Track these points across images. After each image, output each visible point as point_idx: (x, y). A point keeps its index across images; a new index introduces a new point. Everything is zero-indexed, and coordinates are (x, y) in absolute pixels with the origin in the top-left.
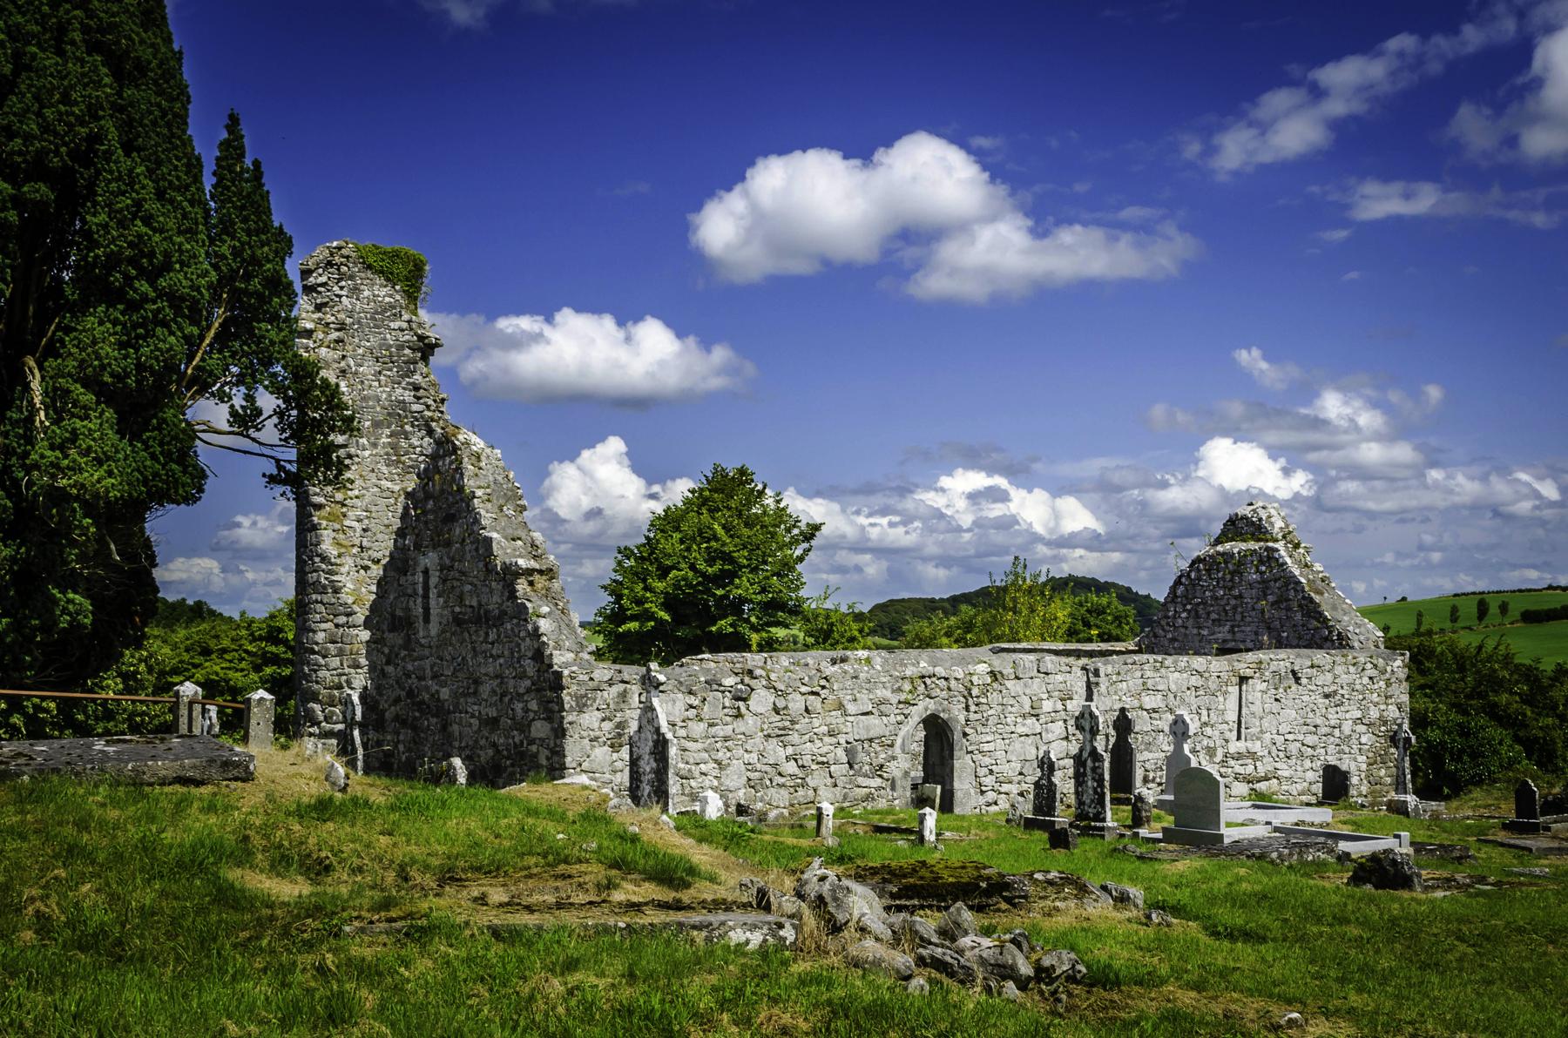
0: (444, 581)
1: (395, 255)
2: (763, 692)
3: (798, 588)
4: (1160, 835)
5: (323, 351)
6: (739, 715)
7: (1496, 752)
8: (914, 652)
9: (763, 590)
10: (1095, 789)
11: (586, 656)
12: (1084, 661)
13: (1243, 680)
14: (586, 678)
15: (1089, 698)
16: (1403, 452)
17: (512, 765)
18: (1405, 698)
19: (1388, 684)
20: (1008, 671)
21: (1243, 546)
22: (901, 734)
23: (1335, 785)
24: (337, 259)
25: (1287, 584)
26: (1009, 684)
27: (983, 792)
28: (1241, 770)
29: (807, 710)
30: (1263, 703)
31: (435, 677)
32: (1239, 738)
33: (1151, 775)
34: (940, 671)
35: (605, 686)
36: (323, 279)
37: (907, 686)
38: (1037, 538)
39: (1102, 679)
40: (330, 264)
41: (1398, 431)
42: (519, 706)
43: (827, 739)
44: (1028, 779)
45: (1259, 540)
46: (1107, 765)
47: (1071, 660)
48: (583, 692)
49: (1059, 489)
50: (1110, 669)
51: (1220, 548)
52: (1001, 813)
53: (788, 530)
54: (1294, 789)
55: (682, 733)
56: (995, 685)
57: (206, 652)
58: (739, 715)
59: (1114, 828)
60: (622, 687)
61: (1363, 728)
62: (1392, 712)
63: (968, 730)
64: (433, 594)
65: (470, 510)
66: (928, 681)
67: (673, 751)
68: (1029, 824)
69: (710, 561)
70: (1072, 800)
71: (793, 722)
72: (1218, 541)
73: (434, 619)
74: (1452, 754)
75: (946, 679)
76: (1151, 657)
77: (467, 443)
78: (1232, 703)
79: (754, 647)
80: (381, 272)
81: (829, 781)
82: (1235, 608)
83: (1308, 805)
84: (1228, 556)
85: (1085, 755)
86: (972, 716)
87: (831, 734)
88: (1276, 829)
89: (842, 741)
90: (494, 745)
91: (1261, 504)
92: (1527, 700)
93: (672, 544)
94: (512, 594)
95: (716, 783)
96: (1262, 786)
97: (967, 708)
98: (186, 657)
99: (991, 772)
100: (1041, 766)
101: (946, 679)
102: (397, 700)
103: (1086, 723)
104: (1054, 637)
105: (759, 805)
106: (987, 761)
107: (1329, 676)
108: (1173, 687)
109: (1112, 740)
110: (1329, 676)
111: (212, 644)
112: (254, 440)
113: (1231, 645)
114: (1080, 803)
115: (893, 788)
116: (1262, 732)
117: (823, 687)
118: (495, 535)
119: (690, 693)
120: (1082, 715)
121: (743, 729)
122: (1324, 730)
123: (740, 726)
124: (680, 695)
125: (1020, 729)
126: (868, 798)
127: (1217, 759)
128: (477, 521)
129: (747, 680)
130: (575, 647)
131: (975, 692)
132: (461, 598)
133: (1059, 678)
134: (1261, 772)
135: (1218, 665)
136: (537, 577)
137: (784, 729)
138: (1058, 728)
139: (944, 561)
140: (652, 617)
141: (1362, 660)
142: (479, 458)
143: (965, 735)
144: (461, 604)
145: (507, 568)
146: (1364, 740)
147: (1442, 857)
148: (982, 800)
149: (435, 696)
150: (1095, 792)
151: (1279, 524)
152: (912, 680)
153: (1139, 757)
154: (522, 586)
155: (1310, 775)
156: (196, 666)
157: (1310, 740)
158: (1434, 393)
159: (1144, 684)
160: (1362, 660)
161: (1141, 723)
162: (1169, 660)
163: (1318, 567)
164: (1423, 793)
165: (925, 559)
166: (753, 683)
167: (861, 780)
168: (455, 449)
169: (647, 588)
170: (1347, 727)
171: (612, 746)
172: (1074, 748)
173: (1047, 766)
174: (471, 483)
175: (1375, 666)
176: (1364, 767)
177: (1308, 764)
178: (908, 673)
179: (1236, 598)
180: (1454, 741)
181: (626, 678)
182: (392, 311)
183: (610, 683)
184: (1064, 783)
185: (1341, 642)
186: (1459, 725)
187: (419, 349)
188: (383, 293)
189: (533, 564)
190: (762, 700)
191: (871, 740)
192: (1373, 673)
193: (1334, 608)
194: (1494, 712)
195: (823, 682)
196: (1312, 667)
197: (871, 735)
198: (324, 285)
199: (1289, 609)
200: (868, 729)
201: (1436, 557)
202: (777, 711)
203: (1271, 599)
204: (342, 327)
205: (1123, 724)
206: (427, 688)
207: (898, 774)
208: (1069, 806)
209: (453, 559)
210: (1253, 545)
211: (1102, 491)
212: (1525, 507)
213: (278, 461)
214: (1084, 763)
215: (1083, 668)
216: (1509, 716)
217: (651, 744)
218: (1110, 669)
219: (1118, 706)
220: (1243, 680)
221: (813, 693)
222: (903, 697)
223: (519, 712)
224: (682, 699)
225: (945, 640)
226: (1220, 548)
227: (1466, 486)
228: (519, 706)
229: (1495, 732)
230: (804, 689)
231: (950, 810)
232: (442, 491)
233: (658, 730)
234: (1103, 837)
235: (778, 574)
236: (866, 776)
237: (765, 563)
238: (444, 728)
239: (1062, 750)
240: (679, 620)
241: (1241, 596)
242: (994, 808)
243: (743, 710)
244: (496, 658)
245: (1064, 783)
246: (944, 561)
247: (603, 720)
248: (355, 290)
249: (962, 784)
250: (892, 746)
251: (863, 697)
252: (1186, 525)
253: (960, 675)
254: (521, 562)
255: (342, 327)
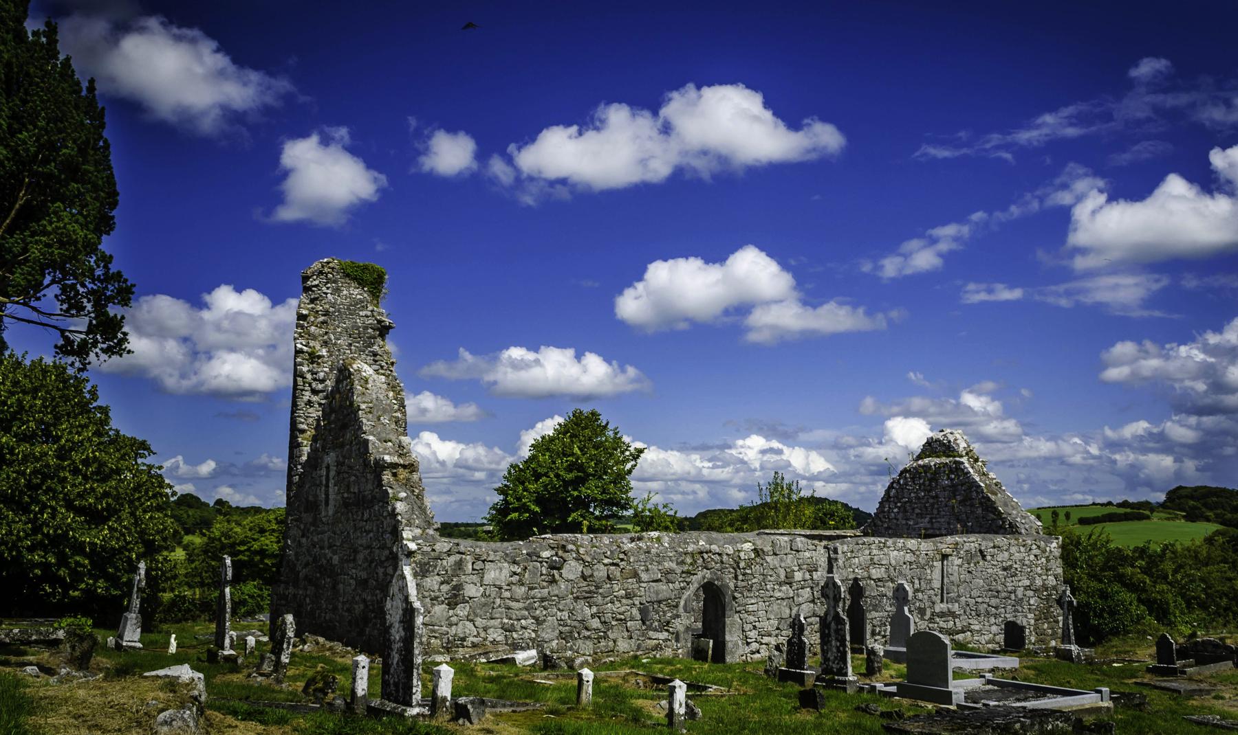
0: (338, 473)
1: (365, 268)
2: (573, 563)
3: (627, 491)
4: (893, 689)
5: (313, 328)
6: (553, 581)
7: (1127, 610)
8: (695, 534)
9: (603, 492)
10: (838, 648)
11: (431, 532)
12: (824, 543)
13: (945, 557)
14: (429, 549)
15: (830, 570)
16: (1011, 426)
17: (375, 617)
18: (1060, 571)
19: (1048, 560)
20: (768, 548)
21: (938, 460)
22: (684, 597)
23: (1014, 638)
24: (326, 270)
25: (970, 488)
26: (769, 559)
27: (748, 644)
28: (942, 624)
29: (608, 577)
30: (960, 574)
31: (330, 547)
32: (942, 601)
33: (878, 629)
34: (714, 548)
35: (444, 556)
36: (316, 282)
37: (689, 560)
38: (799, 475)
39: (840, 555)
40: (321, 273)
41: (1008, 413)
42: (381, 571)
43: (624, 601)
44: (784, 633)
45: (948, 456)
46: (847, 627)
47: (816, 542)
48: (426, 560)
49: (809, 446)
50: (845, 548)
51: (920, 462)
52: (762, 662)
53: (622, 453)
54: (984, 639)
55: (507, 594)
56: (758, 560)
57: (262, 531)
58: (553, 581)
59: (855, 682)
60: (458, 557)
61: (1030, 593)
62: (1051, 581)
63: (736, 594)
64: (332, 482)
65: (357, 420)
66: (705, 556)
67: (419, 620)
68: (784, 677)
69: (569, 469)
70: (818, 649)
71: (597, 587)
72: (919, 457)
73: (331, 503)
74: (1095, 612)
75: (720, 555)
76: (877, 540)
77: (359, 371)
78: (937, 575)
79: (585, 530)
80: (355, 279)
81: (626, 634)
82: (932, 505)
83: (994, 652)
84: (926, 468)
85: (829, 618)
86: (739, 583)
87: (628, 596)
88: (989, 682)
89: (637, 602)
90: (364, 601)
91: (949, 431)
92: (1145, 571)
93: (545, 458)
94: (380, 483)
95: (533, 635)
96: (960, 637)
97: (736, 578)
98: (249, 534)
99: (755, 627)
100: (792, 626)
101: (720, 555)
102: (307, 564)
103: (829, 591)
104: (803, 527)
105: (569, 653)
106: (752, 618)
107: (1006, 554)
108: (893, 562)
109: (848, 603)
110: (1006, 554)
111: (266, 526)
112: (34, 309)
113: (930, 532)
114: (826, 659)
115: (677, 640)
116: (959, 596)
117: (622, 560)
118: (371, 438)
119: (514, 562)
120: (827, 584)
121: (556, 592)
122: (1004, 595)
123: (554, 590)
124: (506, 565)
125: (778, 594)
126: (657, 647)
127: (927, 617)
128: (360, 428)
129: (560, 553)
130: (423, 524)
131: (742, 565)
132: (348, 486)
133: (807, 554)
134: (959, 626)
135: (926, 546)
136: (401, 470)
137: (590, 592)
138: (806, 593)
139: (742, 488)
140: (528, 510)
141: (1029, 542)
142: (367, 381)
143: (735, 598)
144: (348, 491)
145: (377, 462)
146: (1032, 602)
147: (1125, 704)
148: (747, 650)
149: (329, 561)
150: (838, 650)
151: (963, 445)
152: (692, 554)
153: (869, 616)
154: (387, 477)
155: (994, 629)
156: (255, 540)
157: (994, 602)
158: (1025, 392)
159: (872, 559)
160: (1029, 542)
161: (871, 590)
162: (890, 542)
163: (992, 475)
164: (1081, 642)
165: (735, 486)
166: (565, 555)
167: (651, 633)
168: (350, 374)
169: (525, 489)
170: (1020, 592)
171: (448, 604)
172: (821, 609)
173: (797, 627)
174: (359, 399)
175: (1039, 547)
176: (1032, 622)
177: (993, 620)
178: (690, 549)
179: (933, 498)
180: (1096, 602)
181: (462, 549)
182: (362, 304)
183: (449, 553)
184: (812, 638)
185: (1009, 528)
186: (1100, 590)
187: (378, 329)
188: (357, 293)
189: (395, 459)
190: (572, 570)
191: (660, 602)
192: (1037, 552)
193: (1006, 505)
194: (1120, 579)
195: (622, 556)
196: (994, 547)
197: (661, 597)
198: (316, 286)
199: (972, 505)
200: (657, 593)
201: (1026, 486)
202: (584, 577)
203: (959, 498)
204: (326, 313)
205: (856, 590)
206: (325, 555)
207: (681, 629)
208: (815, 654)
209: (344, 457)
210: (944, 460)
211: (834, 447)
212: (1077, 459)
213: (62, 331)
214: (828, 626)
215: (825, 547)
216: (1134, 585)
217: (401, 612)
218: (845, 548)
219: (852, 576)
220: (945, 557)
221: (613, 564)
222: (686, 568)
223: (381, 574)
224: (507, 568)
225: (729, 529)
226: (920, 462)
227: (1045, 447)
228: (381, 571)
229: (1127, 596)
230: (606, 561)
231: (723, 660)
232: (341, 406)
233: (407, 597)
234: (845, 690)
235: (615, 483)
236: (655, 630)
237: (606, 473)
238: (334, 587)
239: (809, 610)
240: (546, 512)
241: (937, 497)
242: (757, 656)
243: (557, 576)
244: (368, 532)
245: (812, 638)
246: (742, 488)
247: (442, 583)
248: (337, 291)
249: (732, 637)
250: (677, 606)
251: (654, 567)
252: (883, 468)
253: (731, 552)
254: (387, 458)
255: (326, 313)
